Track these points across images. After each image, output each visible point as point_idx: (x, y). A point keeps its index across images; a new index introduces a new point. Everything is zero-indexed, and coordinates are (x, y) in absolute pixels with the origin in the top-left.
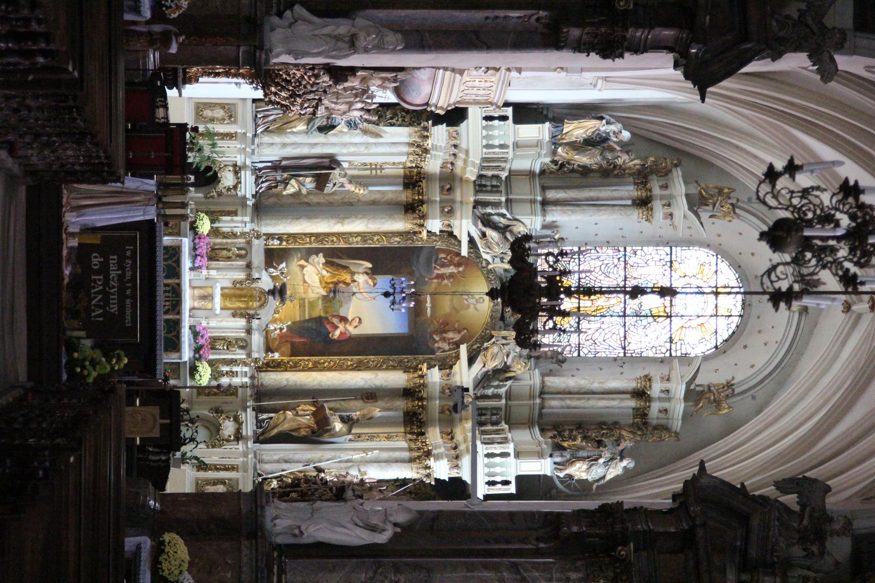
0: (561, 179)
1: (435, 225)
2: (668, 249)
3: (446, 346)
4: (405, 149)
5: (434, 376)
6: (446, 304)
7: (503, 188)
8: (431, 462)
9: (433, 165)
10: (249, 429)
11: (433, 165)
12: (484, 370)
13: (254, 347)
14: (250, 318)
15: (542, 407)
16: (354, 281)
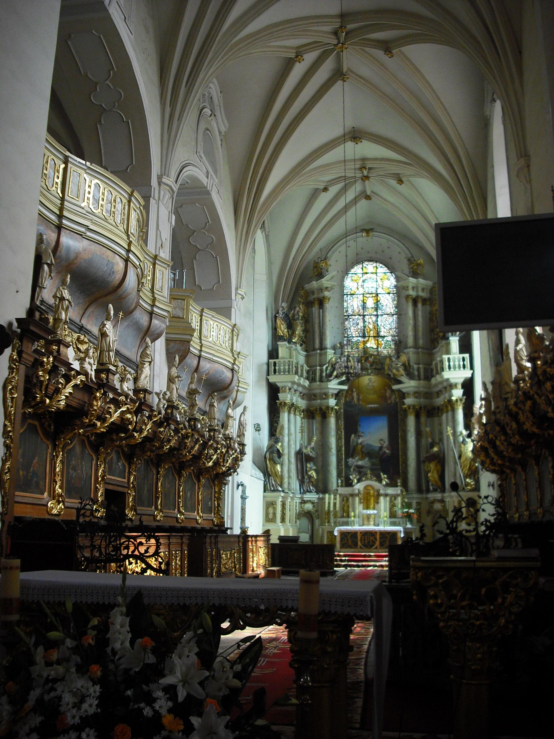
0: (312, 342)
1: (332, 402)
2: (345, 296)
3: (393, 397)
4: (292, 415)
5: (409, 401)
6: (373, 397)
8: (454, 398)
9: (302, 403)
10: (438, 496)
12: (404, 375)
13: (395, 493)
14: (379, 495)
15: (423, 348)
16: (361, 443)
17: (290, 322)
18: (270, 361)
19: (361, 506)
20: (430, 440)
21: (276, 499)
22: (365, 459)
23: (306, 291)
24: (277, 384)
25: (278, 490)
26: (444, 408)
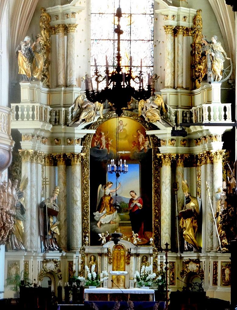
1: (78, 148)
3: (147, 143)
4: (34, 165)
7: (57, 109)
8: (213, 152)
10: (193, 255)
11: (44, 149)
12: (160, 120)
14: (130, 254)
17: (32, 54)
18: (12, 105)
19: (111, 267)
20: (186, 194)
21: (20, 259)
22: (113, 212)
23: (48, 14)
24: (19, 130)
25: (21, 249)
26: (203, 158)
